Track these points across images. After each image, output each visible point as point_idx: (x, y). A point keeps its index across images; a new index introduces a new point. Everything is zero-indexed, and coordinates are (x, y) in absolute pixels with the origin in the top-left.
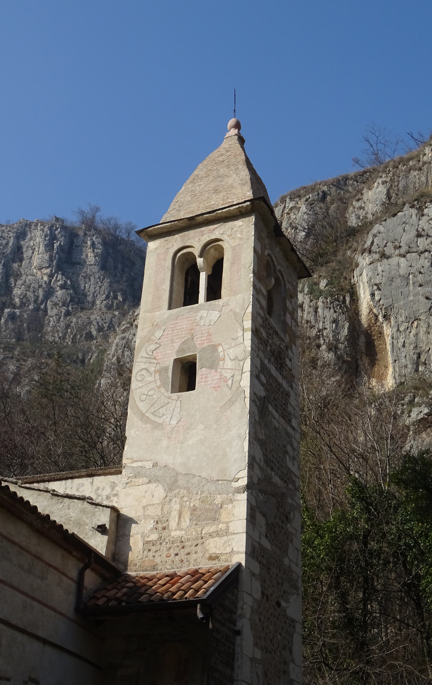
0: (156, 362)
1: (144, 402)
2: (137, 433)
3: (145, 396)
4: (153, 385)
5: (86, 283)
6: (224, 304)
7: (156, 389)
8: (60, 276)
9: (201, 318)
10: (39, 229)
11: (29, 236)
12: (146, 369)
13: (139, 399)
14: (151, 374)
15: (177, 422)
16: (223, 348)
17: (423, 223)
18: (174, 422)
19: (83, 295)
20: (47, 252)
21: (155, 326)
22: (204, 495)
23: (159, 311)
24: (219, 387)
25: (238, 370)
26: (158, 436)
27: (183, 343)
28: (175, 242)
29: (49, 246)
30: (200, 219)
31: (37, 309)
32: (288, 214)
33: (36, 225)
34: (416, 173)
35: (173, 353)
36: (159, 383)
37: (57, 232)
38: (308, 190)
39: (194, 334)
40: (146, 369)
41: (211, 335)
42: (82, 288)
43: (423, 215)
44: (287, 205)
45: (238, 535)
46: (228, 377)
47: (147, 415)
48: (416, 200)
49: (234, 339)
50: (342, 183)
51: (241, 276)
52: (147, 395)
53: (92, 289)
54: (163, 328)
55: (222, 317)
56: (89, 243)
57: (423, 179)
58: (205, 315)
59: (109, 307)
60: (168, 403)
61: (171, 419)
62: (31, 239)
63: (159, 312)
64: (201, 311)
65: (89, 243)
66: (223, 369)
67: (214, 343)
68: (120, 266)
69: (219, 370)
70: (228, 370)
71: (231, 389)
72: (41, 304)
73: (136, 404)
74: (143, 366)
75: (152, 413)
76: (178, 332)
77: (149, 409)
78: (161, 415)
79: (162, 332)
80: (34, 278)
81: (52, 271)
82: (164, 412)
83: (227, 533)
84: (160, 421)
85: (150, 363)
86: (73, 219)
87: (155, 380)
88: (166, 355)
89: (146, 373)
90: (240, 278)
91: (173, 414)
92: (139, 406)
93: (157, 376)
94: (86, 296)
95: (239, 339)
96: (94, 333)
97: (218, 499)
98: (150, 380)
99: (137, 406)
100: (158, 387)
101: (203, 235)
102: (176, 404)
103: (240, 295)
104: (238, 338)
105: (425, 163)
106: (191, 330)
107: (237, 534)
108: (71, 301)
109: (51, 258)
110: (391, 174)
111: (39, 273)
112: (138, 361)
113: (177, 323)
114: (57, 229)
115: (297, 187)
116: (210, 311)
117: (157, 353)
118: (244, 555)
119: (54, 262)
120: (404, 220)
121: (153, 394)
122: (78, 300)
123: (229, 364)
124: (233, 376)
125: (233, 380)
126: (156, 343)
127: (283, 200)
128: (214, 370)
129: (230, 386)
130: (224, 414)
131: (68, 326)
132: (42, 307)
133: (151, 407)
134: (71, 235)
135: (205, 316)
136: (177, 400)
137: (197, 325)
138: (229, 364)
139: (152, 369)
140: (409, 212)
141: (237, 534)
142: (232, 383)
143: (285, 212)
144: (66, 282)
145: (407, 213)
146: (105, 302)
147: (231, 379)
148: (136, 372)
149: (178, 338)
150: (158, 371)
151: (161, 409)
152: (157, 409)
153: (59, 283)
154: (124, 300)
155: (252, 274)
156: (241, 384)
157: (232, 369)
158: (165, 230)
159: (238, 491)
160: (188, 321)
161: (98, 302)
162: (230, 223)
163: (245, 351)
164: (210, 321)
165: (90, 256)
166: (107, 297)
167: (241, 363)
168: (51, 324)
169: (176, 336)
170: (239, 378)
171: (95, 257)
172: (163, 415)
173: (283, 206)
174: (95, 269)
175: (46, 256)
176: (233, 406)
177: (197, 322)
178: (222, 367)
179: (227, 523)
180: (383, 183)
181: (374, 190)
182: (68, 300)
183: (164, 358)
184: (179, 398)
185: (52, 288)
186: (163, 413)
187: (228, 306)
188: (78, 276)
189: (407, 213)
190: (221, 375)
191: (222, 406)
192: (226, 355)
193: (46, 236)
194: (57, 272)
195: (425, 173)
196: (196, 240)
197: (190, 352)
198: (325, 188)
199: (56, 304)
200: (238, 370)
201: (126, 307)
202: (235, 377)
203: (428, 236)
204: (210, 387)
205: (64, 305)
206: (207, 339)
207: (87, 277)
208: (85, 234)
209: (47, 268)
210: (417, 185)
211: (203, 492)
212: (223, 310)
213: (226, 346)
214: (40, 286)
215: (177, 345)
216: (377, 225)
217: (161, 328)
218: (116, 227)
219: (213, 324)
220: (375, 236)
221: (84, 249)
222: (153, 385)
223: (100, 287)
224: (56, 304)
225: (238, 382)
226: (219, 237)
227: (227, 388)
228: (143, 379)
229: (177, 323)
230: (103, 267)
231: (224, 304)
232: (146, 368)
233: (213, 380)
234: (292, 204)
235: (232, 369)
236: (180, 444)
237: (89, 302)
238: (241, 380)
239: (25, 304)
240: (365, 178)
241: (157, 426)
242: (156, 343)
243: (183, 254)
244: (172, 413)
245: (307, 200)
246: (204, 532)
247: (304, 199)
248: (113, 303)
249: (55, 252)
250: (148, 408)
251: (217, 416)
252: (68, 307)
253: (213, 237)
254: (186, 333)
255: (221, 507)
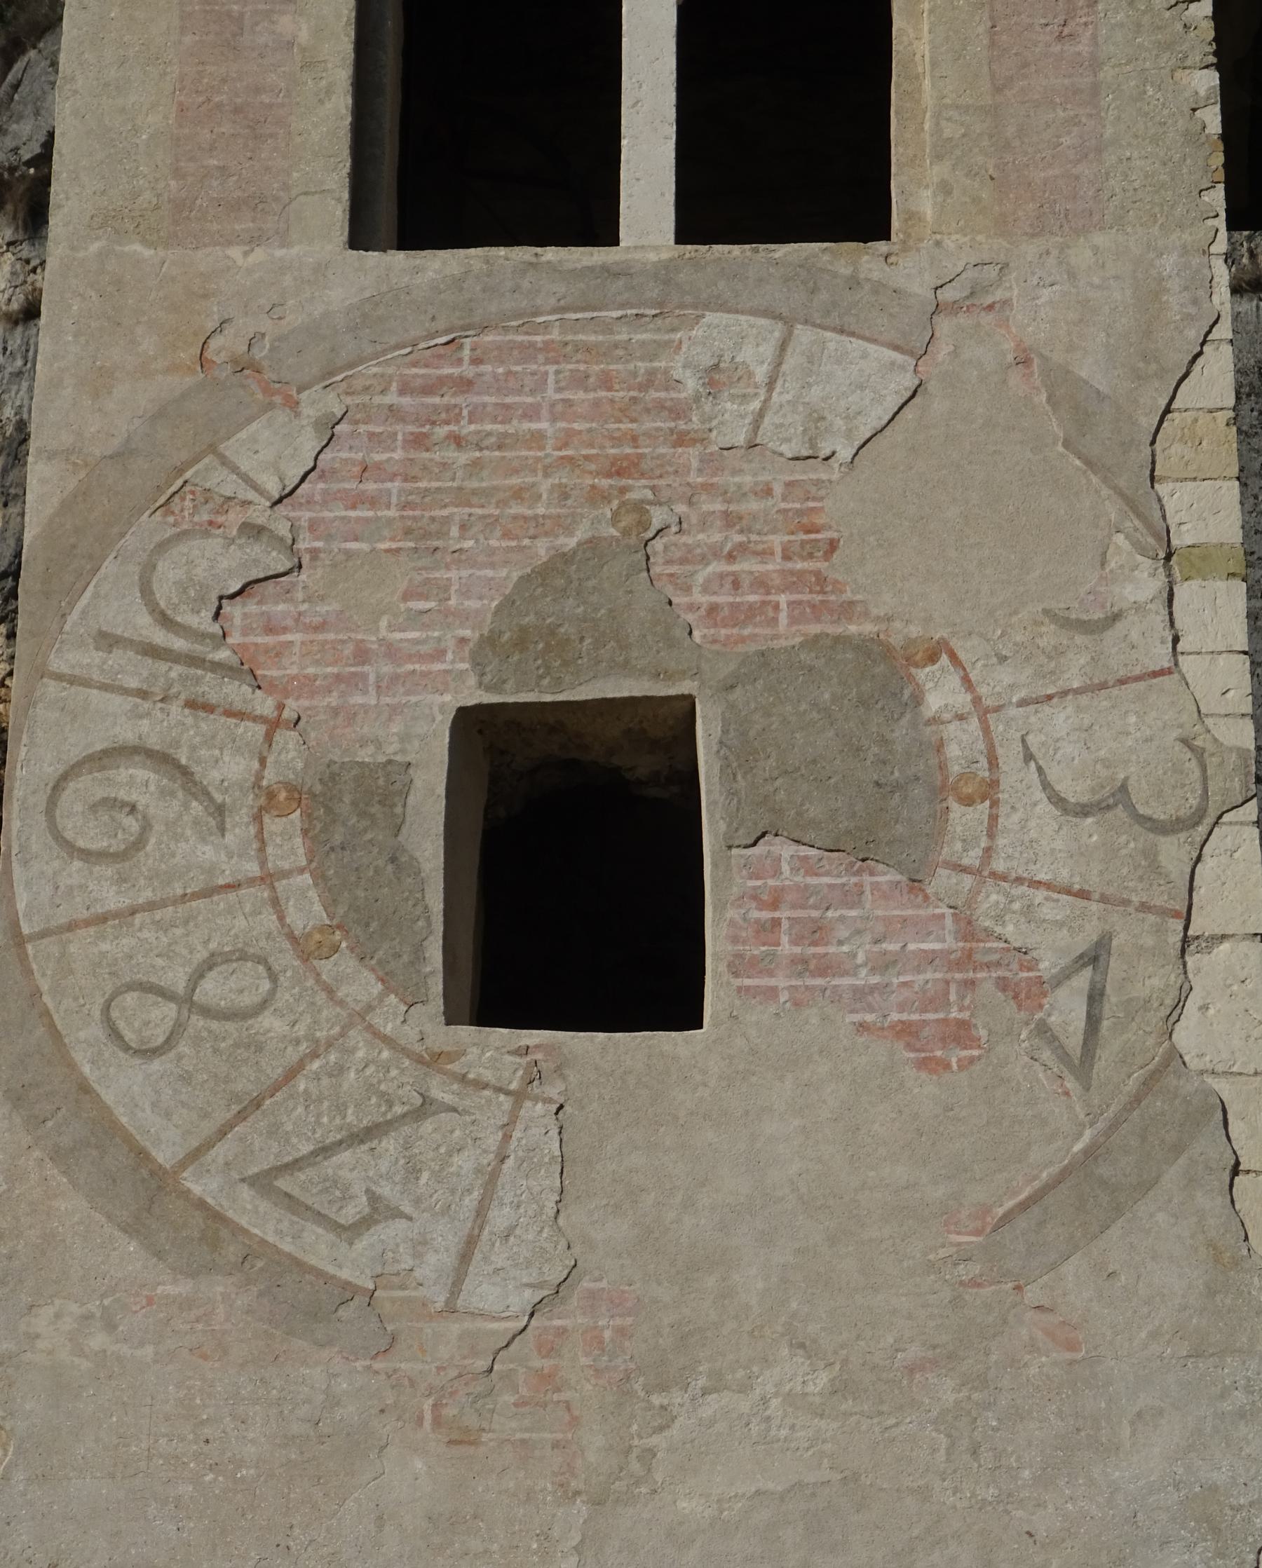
0: (265, 705)
1: (156, 1065)
2: (98, 1340)
3: (171, 1009)
4: (246, 920)
6: (947, 295)
7: (286, 959)
12: (162, 759)
13: (97, 1031)
14: (220, 811)
15: (531, 1296)
16: (967, 682)
18: (498, 1295)
21: (224, 373)
23: (254, 240)
24: (961, 1033)
25: (1144, 907)
26: (333, 1401)
27: (544, 574)
35: (439, 655)
36: (307, 909)
39: (658, 517)
40: (162, 759)
41: (833, 546)
46: (1047, 966)
47: (196, 1185)
49: (1085, 627)
51: (1095, 64)
52: (187, 1001)
54: (321, 402)
55: (937, 404)
58: (756, 357)
60: (426, 1108)
61: (465, 1257)
63: (259, 255)
64: (710, 317)
66: (984, 873)
67: (869, 628)
69: (943, 881)
70: (1040, 895)
71: (1083, 1065)
73: (72, 1066)
74: (118, 721)
75: (252, 1181)
76: (476, 464)
77: (222, 1133)
78: (349, 1214)
79: (309, 444)
82: (385, 1190)
84: (352, 1264)
85: (191, 704)
87: (268, 879)
88: (362, 655)
89: (164, 793)
90: (1095, 90)
91: (481, 1213)
92: (108, 1097)
93: (288, 841)
95: (1131, 627)
98: (211, 870)
99: (85, 1088)
100: (308, 949)
102: (507, 1130)
103: (1099, 239)
104: (1116, 617)
106: (619, 469)
112: (57, 664)
113: (465, 385)
116: (804, 335)
117: (270, 630)
121: (247, 1000)
123: (1037, 837)
124: (1094, 957)
125: (1095, 997)
126: (254, 531)
128: (888, 877)
129: (1074, 1043)
130: (1033, 1294)
133: (241, 1116)
135: (761, 373)
136: (519, 1097)
137: (682, 440)
138: (1037, 837)
139: (229, 769)
142: (1093, 1022)
147: (1083, 980)
148: (51, 770)
149: (491, 523)
150: (296, 793)
151: (345, 1156)
152: (306, 1148)
155: (1211, 79)
156: (1185, 1037)
157: (1083, 895)
160: (580, 381)
163: (1199, 754)
164: (816, 418)
169: (462, 497)
170: (1156, 981)
172: (379, 1211)
176: (1115, 1232)
177: (677, 412)
178: (972, 858)
183: (354, 682)
184: (534, 1076)
186: (373, 1198)
187: (987, 319)
190: (968, 930)
191: (1007, 1218)
192: (1009, 756)
197: (626, 668)
200: (1144, 907)
202: (1116, 967)
204: (862, 1027)
206: (794, 581)
212: (942, 350)
213: (1005, 676)
215: (479, 586)
217: (293, 405)
219: (845, 454)
222: (246, 920)
225: (1155, 1018)
227: (1046, 1055)
228: (138, 844)
229: (465, 385)
231: (947, 295)
232: (154, 742)
233: (884, 964)
235: (1083, 895)
236: (580, 1508)
238: (1180, 1004)
241: (310, 1306)
242: (254, 531)
244: (471, 1201)
250: (208, 1128)
251: (956, 1302)
254: (563, 494)
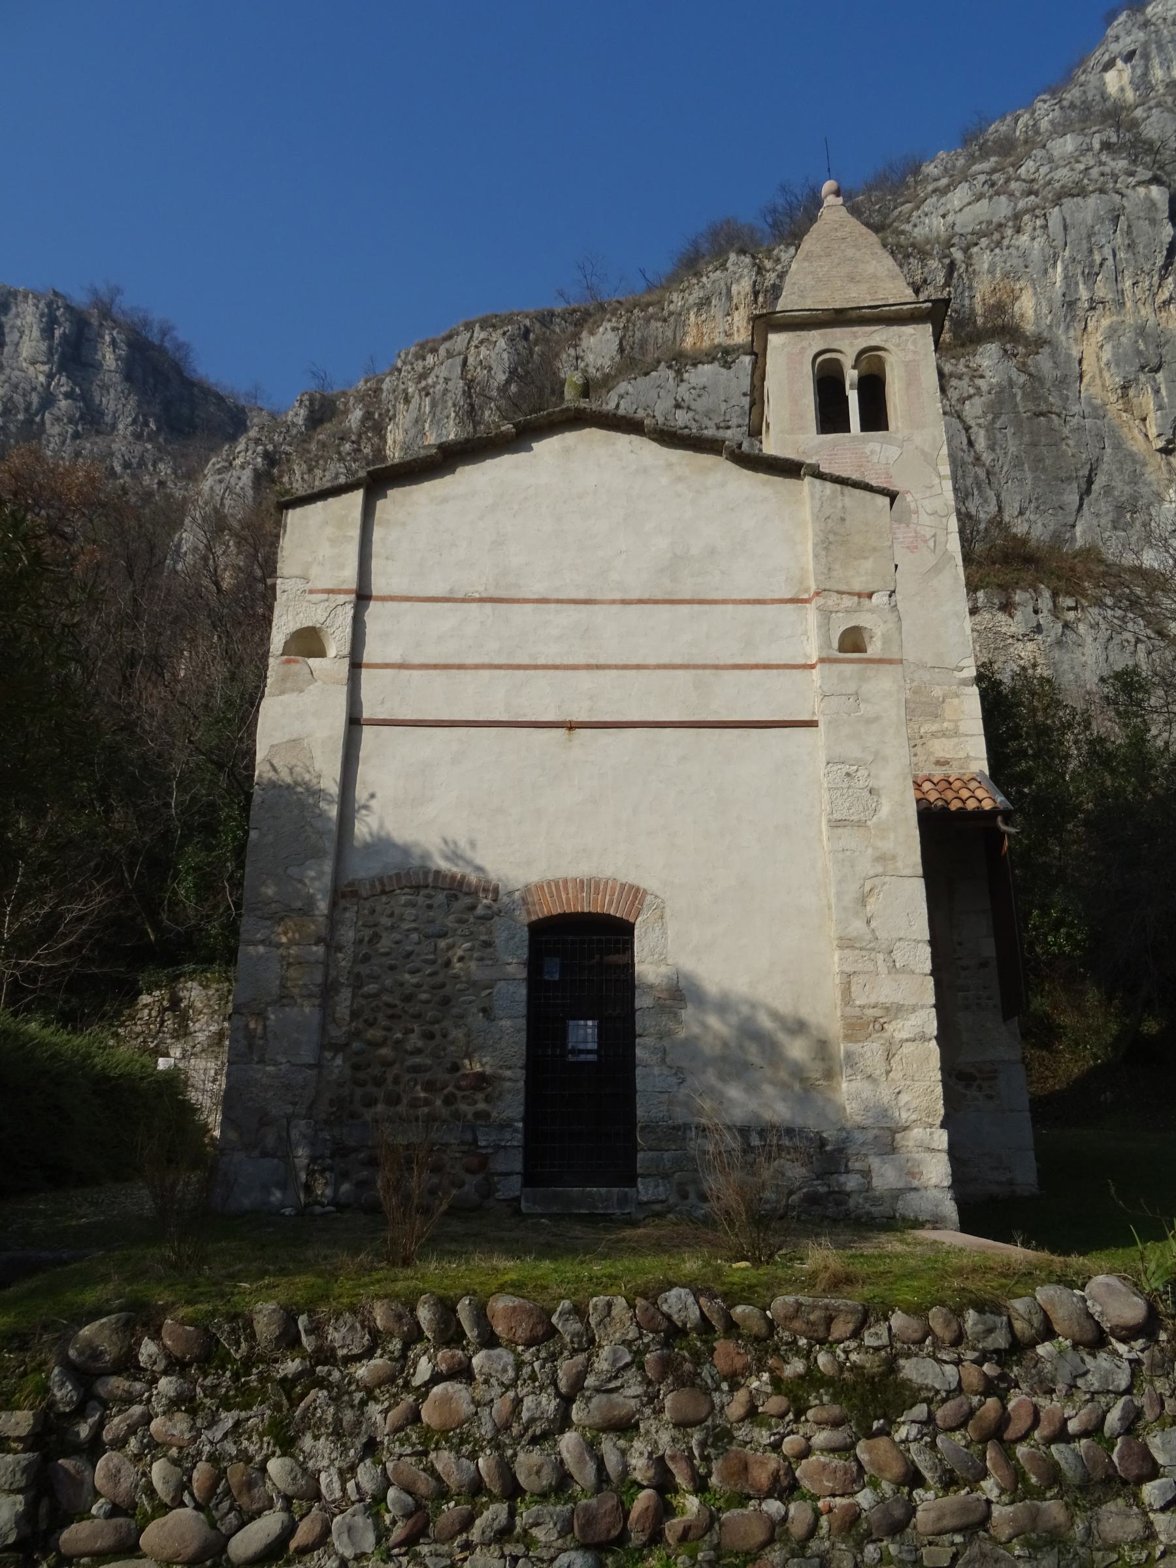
5: (102, 395)
8: (64, 380)
9: (872, 452)
10: (30, 302)
11: (14, 310)
17: (683, 390)
19: (98, 412)
20: (44, 340)
22: (915, 684)
24: (916, 547)
28: (815, 340)
29: (47, 332)
30: (854, 314)
31: (29, 421)
32: (476, 347)
33: (26, 297)
34: (659, 324)
37: (58, 313)
38: (509, 320)
42: (97, 402)
43: (682, 381)
44: (475, 335)
45: (974, 738)
48: (674, 359)
50: (548, 319)
53: (112, 407)
56: (107, 338)
57: (669, 334)
59: (138, 437)
62: (17, 315)
65: (107, 338)
66: (918, 524)
68: (151, 380)
72: (36, 415)
80: (23, 374)
81: (51, 369)
83: (956, 733)
86: (80, 298)
94: (103, 414)
96: (118, 469)
97: (938, 692)
101: (856, 337)
105: (671, 314)
107: (972, 735)
108: (82, 418)
109: (50, 348)
110: (624, 319)
111: (32, 368)
114: (58, 308)
115: (489, 313)
118: (986, 763)
119: (56, 357)
120: (659, 382)
122: (91, 419)
123: (924, 518)
124: (934, 536)
127: (469, 326)
131: (78, 454)
132: (38, 419)
134: (80, 321)
140: (664, 374)
141: (972, 735)
143: (473, 344)
144: (73, 390)
145: (663, 374)
146: (131, 428)
153: (63, 389)
154: (159, 429)
158: (799, 320)
159: (964, 683)
161: (121, 426)
162: (895, 328)
165: (109, 359)
166: (134, 422)
167: (944, 520)
168: (52, 446)
170: (944, 539)
171: (117, 360)
173: (469, 335)
174: (117, 378)
175: (43, 346)
179: (956, 721)
180: (613, 329)
181: (598, 336)
182: (77, 415)
185: (51, 394)
188: (91, 383)
189: (663, 374)
190: (916, 532)
193: (42, 315)
194: (59, 372)
195: (672, 327)
196: (848, 344)
198: (527, 322)
199: (58, 419)
201: (161, 440)
203: (689, 408)
205: (70, 421)
207: (105, 388)
208: (101, 325)
209: (43, 363)
210: (660, 341)
211: (912, 681)
214: (34, 389)
216: (625, 383)
218: (145, 323)
220: (621, 397)
221: (99, 346)
223: (124, 406)
224: (58, 419)
226: (882, 344)
230: (128, 377)
234: (483, 335)
237: (107, 424)
239: (10, 411)
240: (583, 319)
243: (824, 360)
245: (504, 334)
246: (922, 731)
247: (500, 331)
248: (142, 431)
249: (56, 341)
252: (76, 425)
253: (873, 343)
255: (943, 702)
